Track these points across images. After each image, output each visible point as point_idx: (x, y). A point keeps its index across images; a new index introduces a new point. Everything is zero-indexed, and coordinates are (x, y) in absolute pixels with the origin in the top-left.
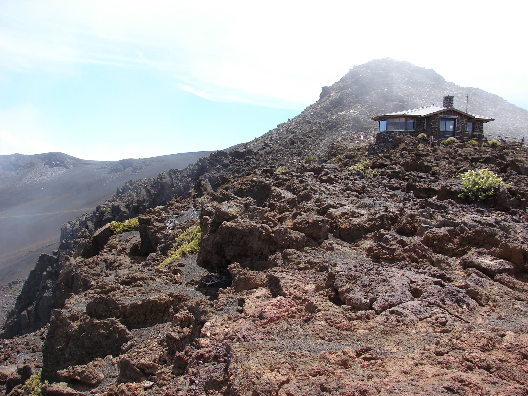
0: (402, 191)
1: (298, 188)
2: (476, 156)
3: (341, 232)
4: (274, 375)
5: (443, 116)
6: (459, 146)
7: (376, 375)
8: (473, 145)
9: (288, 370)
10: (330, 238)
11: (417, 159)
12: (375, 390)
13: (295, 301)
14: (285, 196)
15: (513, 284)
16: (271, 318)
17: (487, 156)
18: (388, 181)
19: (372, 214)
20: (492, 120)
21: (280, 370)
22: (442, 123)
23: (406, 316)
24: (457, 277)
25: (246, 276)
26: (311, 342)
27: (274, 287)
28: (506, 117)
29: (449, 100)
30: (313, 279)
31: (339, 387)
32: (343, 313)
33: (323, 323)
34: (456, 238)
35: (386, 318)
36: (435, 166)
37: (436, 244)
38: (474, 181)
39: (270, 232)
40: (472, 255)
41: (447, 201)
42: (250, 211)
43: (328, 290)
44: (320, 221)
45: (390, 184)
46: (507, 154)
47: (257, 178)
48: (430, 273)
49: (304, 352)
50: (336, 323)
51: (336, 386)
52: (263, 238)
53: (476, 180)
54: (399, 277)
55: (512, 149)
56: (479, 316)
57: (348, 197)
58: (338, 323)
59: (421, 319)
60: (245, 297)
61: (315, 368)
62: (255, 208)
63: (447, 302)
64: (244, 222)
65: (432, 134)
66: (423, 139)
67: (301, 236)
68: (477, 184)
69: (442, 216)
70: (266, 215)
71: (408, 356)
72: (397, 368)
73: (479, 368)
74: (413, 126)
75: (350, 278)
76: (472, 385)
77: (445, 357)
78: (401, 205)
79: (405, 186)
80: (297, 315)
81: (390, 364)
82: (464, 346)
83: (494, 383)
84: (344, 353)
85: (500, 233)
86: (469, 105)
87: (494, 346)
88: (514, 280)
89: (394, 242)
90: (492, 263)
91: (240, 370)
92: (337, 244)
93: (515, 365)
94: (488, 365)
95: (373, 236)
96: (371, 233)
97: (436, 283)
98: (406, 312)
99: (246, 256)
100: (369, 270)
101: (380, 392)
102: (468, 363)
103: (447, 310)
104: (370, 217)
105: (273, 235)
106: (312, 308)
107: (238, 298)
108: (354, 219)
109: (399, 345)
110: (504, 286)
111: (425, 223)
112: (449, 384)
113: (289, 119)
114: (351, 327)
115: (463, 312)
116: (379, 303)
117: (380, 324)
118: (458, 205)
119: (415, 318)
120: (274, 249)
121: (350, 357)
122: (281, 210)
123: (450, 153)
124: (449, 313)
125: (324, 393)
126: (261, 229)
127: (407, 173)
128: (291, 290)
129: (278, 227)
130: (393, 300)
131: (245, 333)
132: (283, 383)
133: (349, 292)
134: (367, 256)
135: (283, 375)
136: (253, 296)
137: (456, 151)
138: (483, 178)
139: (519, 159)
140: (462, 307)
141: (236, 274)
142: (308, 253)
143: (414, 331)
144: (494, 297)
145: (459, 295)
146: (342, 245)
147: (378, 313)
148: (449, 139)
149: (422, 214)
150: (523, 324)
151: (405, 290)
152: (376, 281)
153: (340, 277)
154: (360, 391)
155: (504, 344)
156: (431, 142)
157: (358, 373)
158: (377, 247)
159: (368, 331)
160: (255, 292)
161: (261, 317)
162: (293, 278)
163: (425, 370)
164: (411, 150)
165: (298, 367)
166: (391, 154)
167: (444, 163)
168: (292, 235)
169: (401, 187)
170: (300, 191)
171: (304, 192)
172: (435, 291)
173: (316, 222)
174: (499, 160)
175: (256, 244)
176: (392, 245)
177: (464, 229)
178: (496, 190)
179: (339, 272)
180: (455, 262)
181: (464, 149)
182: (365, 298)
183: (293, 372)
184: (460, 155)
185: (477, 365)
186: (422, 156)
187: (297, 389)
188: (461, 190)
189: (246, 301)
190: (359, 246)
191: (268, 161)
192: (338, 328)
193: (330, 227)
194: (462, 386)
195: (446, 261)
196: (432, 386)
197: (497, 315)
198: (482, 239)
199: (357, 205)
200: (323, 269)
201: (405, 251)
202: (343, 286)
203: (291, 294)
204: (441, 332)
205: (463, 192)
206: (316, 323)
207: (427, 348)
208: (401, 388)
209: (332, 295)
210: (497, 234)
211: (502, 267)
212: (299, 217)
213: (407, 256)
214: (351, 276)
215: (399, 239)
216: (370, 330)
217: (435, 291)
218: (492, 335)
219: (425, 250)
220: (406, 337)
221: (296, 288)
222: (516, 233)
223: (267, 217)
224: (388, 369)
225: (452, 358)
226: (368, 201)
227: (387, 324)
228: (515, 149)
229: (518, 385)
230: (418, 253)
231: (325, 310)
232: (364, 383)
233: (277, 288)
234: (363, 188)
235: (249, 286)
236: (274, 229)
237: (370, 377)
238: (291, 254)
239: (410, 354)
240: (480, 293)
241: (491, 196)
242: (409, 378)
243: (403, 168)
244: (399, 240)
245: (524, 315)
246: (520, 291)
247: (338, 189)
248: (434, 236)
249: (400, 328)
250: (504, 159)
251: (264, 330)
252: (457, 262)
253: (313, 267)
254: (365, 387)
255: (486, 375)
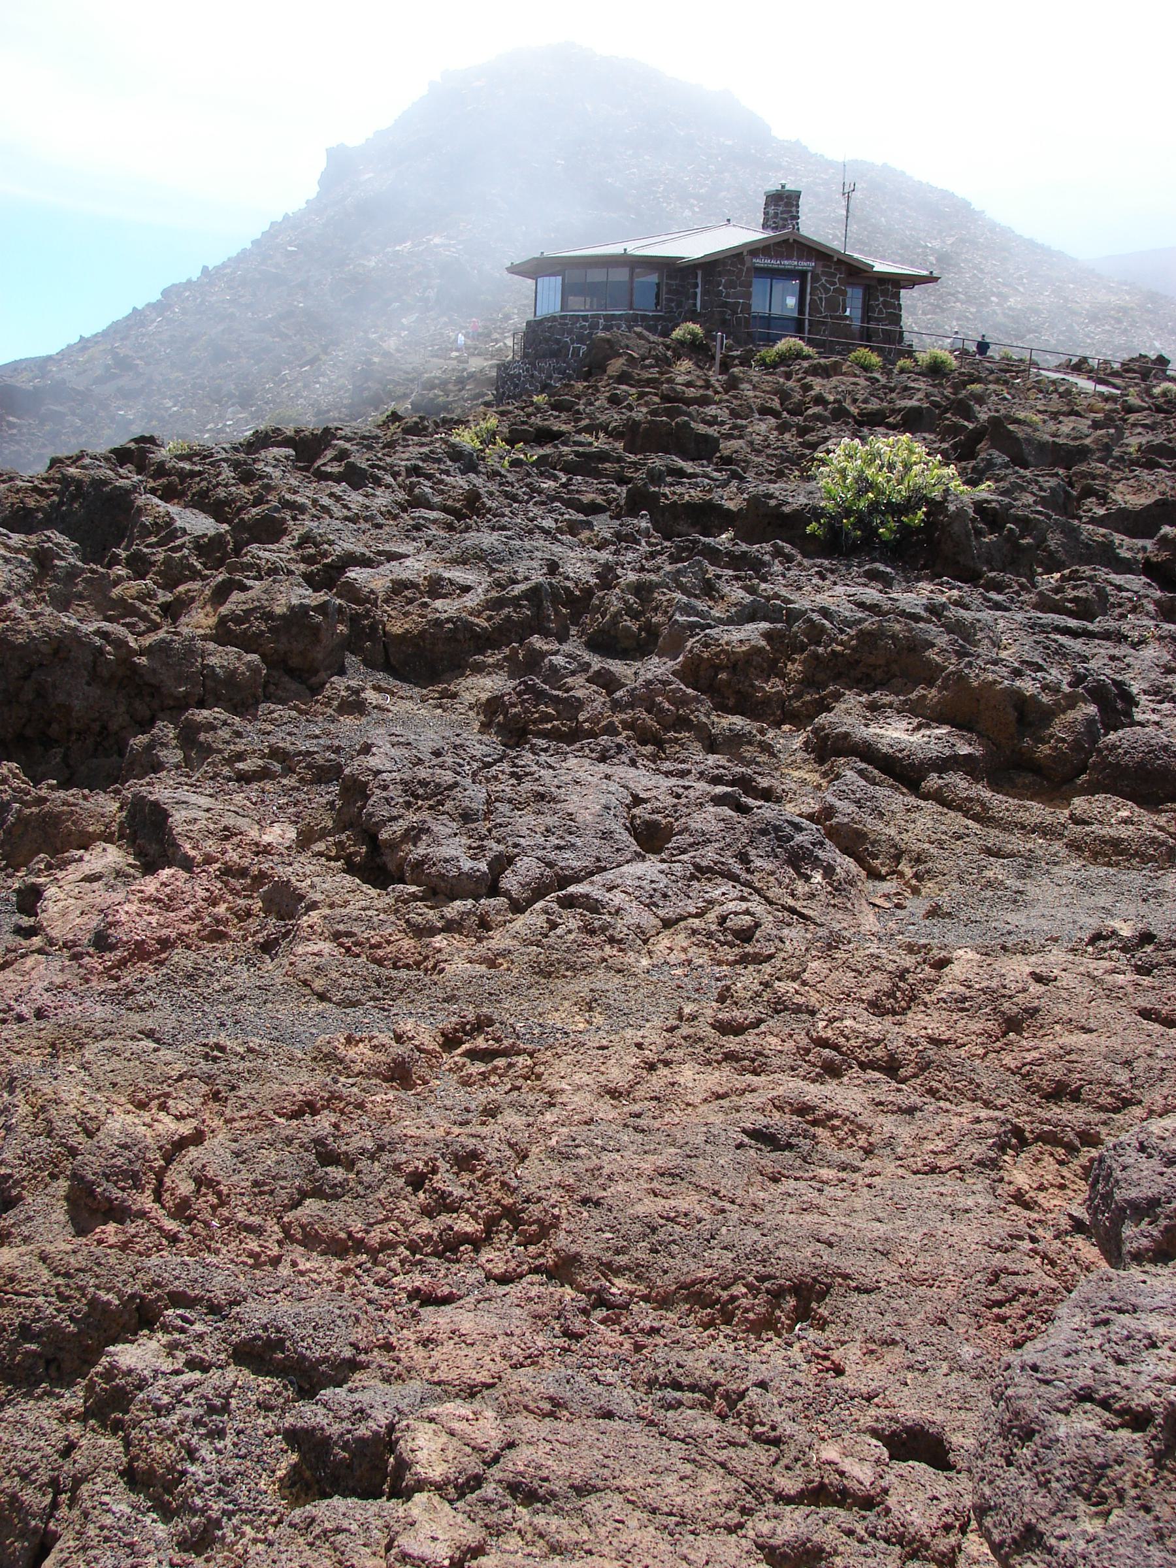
0: (611, 518)
1: (234, 501)
2: (874, 405)
3: (392, 650)
4: (148, 1120)
5: (761, 262)
6: (815, 371)
7: (511, 1105)
8: (866, 368)
9: (197, 1101)
10: (350, 671)
11: (670, 413)
12: (509, 1153)
13: (226, 883)
14: (188, 526)
15: (983, 805)
16: (140, 944)
17: (913, 403)
18: (564, 485)
19: (499, 585)
20: (931, 279)
21: (171, 1102)
22: (759, 287)
23: (617, 912)
24: (793, 786)
25: (46, 807)
26: (284, 1012)
27: (150, 839)
28: (982, 271)
29: (783, 205)
30: (292, 810)
31: (381, 1148)
32: (397, 911)
33: (326, 947)
34: (794, 661)
35: (548, 921)
36: (729, 437)
37: (725, 681)
38: (860, 478)
39: (133, 652)
40: (847, 715)
41: (767, 547)
42: (56, 579)
43: (343, 837)
44: (315, 609)
45: (569, 492)
46: (980, 399)
47: (84, 467)
48: (701, 773)
49: (254, 1042)
50: (372, 947)
51: (370, 1145)
52: (106, 674)
53: (870, 472)
54: (590, 788)
55: (997, 381)
56: (867, 908)
57: (417, 528)
58: (378, 946)
59: (667, 924)
60: (42, 880)
61: (295, 1089)
62: (74, 566)
63: (758, 863)
64: (33, 616)
65: (724, 324)
66: (693, 342)
67: (248, 664)
68: (871, 486)
69: (745, 588)
70: (116, 592)
71: (623, 1038)
72: (586, 1079)
73: (863, 1066)
74: (657, 296)
75: (421, 791)
76: (836, 1122)
77: (751, 1037)
78: (604, 556)
79: (622, 502)
80: (233, 932)
81: (561, 1067)
82: (814, 999)
83: (911, 1111)
84: (399, 1038)
85: (943, 640)
86: (853, 227)
87: (913, 998)
88: (987, 794)
89: (580, 680)
90: (912, 739)
91: (24, 1109)
92: (377, 689)
93: (981, 1051)
94: (892, 1056)
95: (505, 658)
96: (499, 648)
97: (718, 800)
98: (618, 898)
99: (48, 742)
100: (488, 765)
101: (526, 1157)
102: (827, 1052)
103: (758, 891)
104: (494, 594)
105: (144, 660)
106: (285, 902)
107: (17, 886)
108: (439, 604)
109: (591, 1009)
110: (952, 814)
111: (688, 610)
112: (761, 1121)
113: (205, 269)
114: (426, 958)
115: (812, 896)
116: (522, 871)
117: (527, 943)
118: (806, 562)
119: (648, 920)
120: (148, 713)
121: (421, 1051)
122: (173, 576)
123: (784, 395)
124: (766, 899)
125: (329, 1169)
126: (98, 641)
127: (632, 458)
128: (211, 846)
129: (161, 634)
130: (571, 860)
131: (46, 999)
132: (181, 1144)
133: (416, 840)
134: (485, 727)
135: (180, 1118)
136: (73, 873)
137: (807, 388)
138: (891, 467)
139: (1021, 415)
140: (808, 878)
141: (9, 803)
142: (272, 721)
143: (645, 962)
144: (916, 847)
145: (799, 838)
146: (393, 694)
147: (518, 907)
148: (782, 345)
149: (676, 581)
150: (1009, 927)
151: (614, 827)
152: (510, 801)
153: (385, 788)
154: (455, 1155)
155: (946, 988)
156: (718, 356)
157: (448, 1103)
158: (519, 694)
159: (484, 967)
160: (81, 859)
161: (102, 942)
162: (218, 806)
163: (682, 1081)
164: (649, 382)
165: (233, 1088)
166: (578, 397)
167: (762, 427)
168: (213, 661)
169: (610, 503)
170: (241, 509)
171: (254, 511)
172: (715, 827)
173: (299, 613)
174: (951, 418)
175: (80, 697)
176: (571, 689)
177: (822, 630)
178: (936, 507)
179: (379, 772)
180: (791, 741)
181: (834, 380)
182: (474, 858)
183: (216, 1106)
184: (819, 400)
185: (856, 1059)
186: (689, 402)
187: (230, 1161)
188: (815, 508)
189: (47, 894)
190: (454, 696)
191: (131, 422)
192: (379, 962)
193: (351, 628)
194: (805, 1126)
195: (759, 737)
196: (704, 1129)
197: (926, 905)
198: (882, 662)
199: (447, 554)
200: (325, 774)
201: (616, 706)
202: (394, 819)
203: (209, 860)
204: (736, 962)
205: (823, 515)
206: (300, 950)
207: (687, 1010)
208: (599, 1142)
209: (356, 853)
210: (933, 645)
211: (947, 752)
212: (236, 596)
213: (622, 722)
214: (423, 783)
215: (596, 667)
216: (492, 964)
217: (715, 827)
218: (909, 961)
219: (684, 701)
220: (617, 980)
221: (227, 838)
222: (996, 644)
223: (122, 600)
224: (554, 1084)
225: (773, 1040)
226: (488, 539)
227: (551, 941)
228: (1006, 382)
229: (984, 1113)
230: (661, 710)
231: (331, 906)
232: (467, 1130)
233: (161, 842)
234: (473, 498)
235: (58, 839)
236: (148, 640)
237: (491, 1112)
238: (211, 727)
239: (629, 1033)
240: (872, 837)
241: (919, 530)
242: (625, 1109)
243: (620, 445)
244: (598, 673)
245: (1015, 901)
246: (1006, 826)
247: (382, 499)
248: (717, 655)
249: (596, 954)
250: (969, 415)
251: (114, 985)
252: (798, 742)
253: (289, 770)
254: (471, 1143)
255: (885, 1089)
